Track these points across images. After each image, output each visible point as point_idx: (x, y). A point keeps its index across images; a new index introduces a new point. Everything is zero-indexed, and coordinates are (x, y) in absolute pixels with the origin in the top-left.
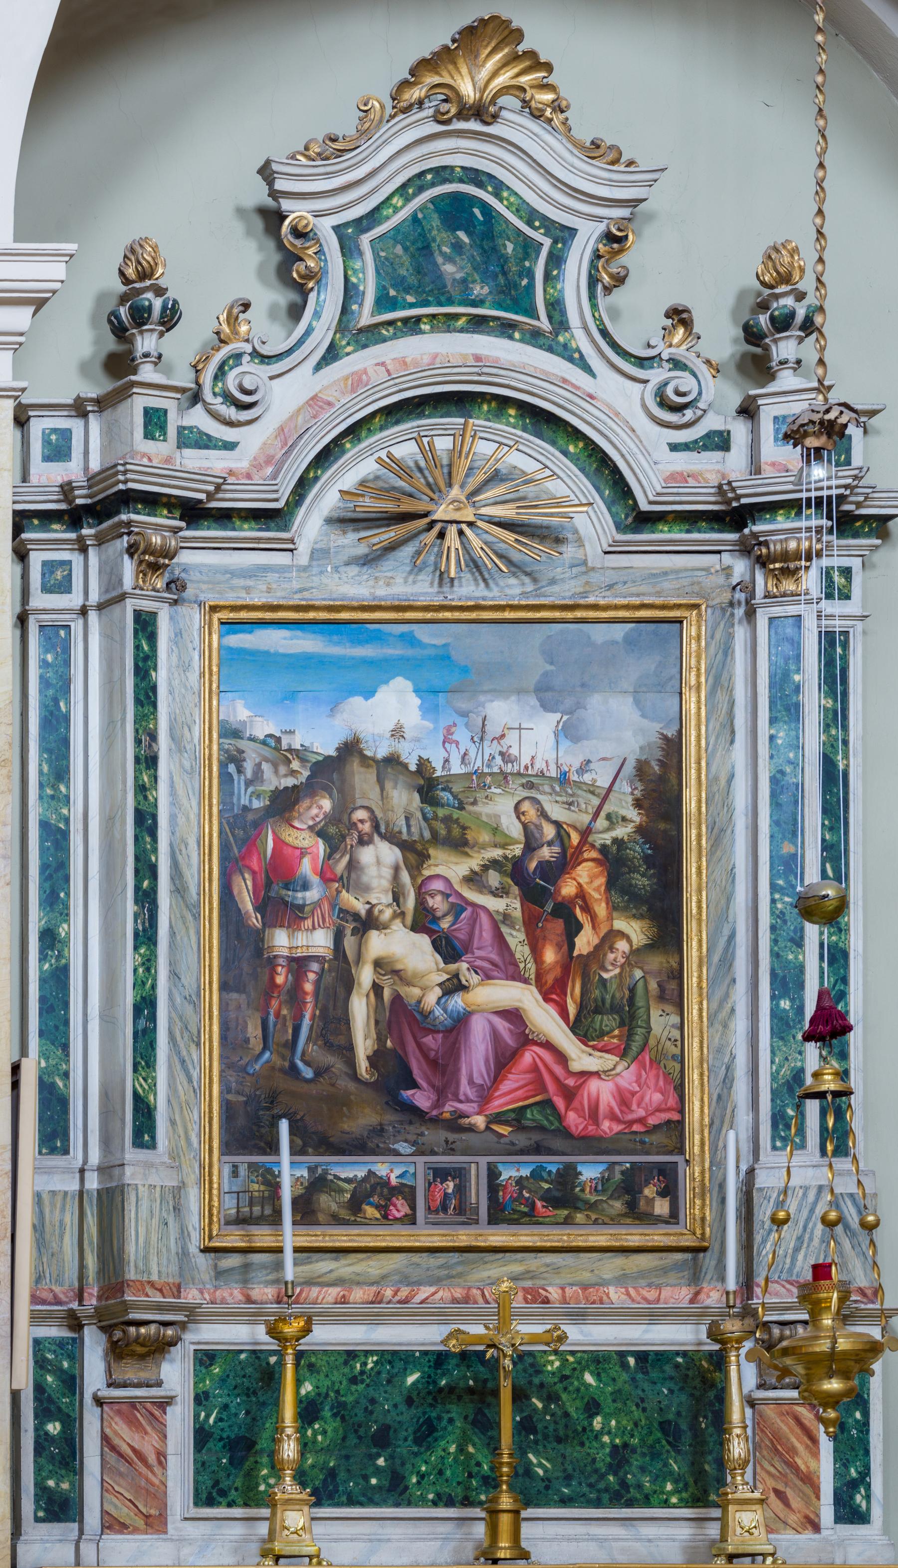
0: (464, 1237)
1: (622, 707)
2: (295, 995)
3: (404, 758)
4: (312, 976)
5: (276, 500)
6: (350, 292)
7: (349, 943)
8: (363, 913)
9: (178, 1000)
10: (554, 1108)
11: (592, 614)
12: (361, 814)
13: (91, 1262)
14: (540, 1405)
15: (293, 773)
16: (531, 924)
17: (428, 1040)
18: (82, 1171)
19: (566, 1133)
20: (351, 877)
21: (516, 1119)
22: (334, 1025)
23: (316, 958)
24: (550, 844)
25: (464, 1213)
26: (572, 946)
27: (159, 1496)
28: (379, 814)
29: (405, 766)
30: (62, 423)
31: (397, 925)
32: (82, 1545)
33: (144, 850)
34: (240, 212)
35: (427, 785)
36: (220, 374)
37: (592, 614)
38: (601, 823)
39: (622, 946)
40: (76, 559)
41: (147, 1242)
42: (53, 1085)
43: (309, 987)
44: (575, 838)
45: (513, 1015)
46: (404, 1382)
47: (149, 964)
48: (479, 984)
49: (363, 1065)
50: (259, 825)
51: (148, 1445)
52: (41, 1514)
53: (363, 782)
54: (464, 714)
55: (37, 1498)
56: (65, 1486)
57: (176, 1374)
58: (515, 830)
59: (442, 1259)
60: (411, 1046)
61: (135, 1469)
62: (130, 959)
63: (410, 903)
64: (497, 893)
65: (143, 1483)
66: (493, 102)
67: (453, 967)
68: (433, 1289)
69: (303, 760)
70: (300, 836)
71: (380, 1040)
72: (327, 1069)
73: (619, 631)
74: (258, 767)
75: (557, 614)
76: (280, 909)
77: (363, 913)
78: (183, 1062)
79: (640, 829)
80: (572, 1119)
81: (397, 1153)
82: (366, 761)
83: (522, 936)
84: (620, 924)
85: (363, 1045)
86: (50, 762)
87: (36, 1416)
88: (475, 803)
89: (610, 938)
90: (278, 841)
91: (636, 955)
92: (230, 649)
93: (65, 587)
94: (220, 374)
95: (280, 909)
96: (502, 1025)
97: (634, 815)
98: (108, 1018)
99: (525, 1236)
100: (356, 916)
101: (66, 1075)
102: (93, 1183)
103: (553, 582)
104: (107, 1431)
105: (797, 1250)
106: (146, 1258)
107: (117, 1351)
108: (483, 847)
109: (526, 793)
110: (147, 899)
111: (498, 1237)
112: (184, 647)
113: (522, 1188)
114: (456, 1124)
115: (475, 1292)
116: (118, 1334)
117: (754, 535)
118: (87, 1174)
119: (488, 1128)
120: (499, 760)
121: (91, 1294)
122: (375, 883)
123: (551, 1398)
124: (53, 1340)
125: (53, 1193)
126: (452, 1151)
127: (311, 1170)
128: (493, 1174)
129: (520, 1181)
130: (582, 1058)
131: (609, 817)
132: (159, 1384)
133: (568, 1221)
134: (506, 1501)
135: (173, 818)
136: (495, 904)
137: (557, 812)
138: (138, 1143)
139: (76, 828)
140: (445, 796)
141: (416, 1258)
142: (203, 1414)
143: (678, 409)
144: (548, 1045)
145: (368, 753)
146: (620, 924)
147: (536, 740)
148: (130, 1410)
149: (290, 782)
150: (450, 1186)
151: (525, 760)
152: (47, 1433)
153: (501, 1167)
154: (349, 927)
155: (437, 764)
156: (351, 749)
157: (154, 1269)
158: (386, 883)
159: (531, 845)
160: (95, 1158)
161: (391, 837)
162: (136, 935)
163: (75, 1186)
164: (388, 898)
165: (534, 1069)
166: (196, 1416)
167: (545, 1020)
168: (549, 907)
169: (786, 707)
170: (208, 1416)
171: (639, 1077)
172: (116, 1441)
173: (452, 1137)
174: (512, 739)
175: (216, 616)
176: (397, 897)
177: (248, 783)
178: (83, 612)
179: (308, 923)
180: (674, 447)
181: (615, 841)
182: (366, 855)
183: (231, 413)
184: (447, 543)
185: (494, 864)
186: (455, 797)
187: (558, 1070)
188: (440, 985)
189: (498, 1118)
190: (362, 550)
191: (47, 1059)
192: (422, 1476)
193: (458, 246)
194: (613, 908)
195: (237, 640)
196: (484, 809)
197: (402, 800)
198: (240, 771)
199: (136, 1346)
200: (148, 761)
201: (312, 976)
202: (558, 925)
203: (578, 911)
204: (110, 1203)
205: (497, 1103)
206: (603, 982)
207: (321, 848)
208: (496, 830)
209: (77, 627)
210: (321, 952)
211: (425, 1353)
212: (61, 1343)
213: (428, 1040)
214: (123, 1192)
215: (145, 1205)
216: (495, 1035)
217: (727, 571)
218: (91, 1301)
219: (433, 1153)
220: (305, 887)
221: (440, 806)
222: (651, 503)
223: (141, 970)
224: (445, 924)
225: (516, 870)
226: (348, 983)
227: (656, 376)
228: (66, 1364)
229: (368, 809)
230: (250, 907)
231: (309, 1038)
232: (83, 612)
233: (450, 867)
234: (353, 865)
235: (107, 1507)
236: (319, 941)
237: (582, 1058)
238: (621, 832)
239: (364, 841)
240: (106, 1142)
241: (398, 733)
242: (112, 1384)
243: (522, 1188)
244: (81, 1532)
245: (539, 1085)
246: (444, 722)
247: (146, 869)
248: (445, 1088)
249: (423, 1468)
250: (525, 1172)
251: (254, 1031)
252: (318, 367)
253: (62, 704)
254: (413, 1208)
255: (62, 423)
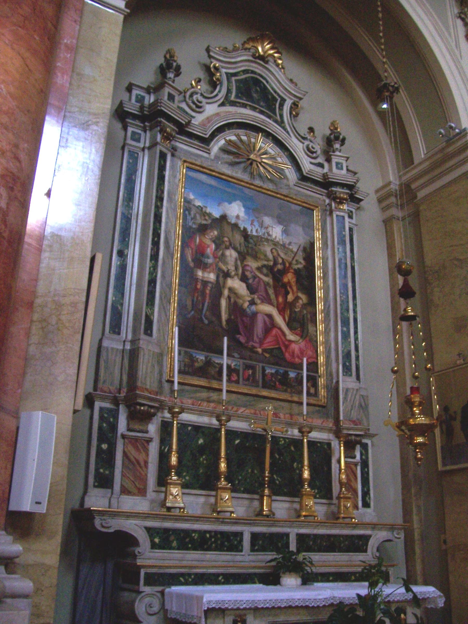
0: (254, 391)
1: (300, 230)
2: (203, 293)
3: (240, 225)
4: (209, 288)
5: (205, 134)
6: (229, 91)
7: (221, 279)
8: (226, 271)
9: (164, 285)
10: (282, 351)
11: (291, 200)
12: (226, 239)
13: (125, 378)
14: (277, 456)
15: (206, 220)
16: (275, 287)
17: (244, 319)
18: (124, 342)
19: (284, 359)
20: (223, 258)
21: (270, 351)
22: (215, 307)
23: (210, 282)
24: (281, 264)
25: (254, 383)
26: (287, 298)
27: (144, 480)
28: (231, 239)
29: (240, 228)
30: (143, 94)
31: (236, 278)
32: (112, 499)
33: (156, 228)
34: (199, 63)
35: (245, 235)
36: (191, 96)
37: (291, 200)
38: (294, 262)
39: (300, 302)
40: (143, 134)
41: (146, 373)
42: (117, 308)
43: (208, 292)
44: (287, 265)
45: (270, 316)
46: (234, 442)
47: (155, 267)
48: (260, 304)
49: (224, 323)
50: (194, 234)
51: (141, 457)
52: (96, 484)
53: (227, 229)
54: (257, 218)
55: (95, 478)
56: (107, 472)
57: (153, 428)
58: (271, 257)
59: (248, 398)
60: (239, 320)
61: (135, 467)
62: (148, 264)
63: (240, 271)
64: (266, 275)
65: (138, 474)
66: (267, 57)
67: (252, 296)
68: (244, 409)
69: (210, 217)
70: (207, 240)
71: (230, 315)
72: (212, 322)
73: (299, 208)
74: (195, 214)
75: (282, 197)
76: (200, 262)
77: (226, 271)
78: (164, 308)
79: (304, 267)
80: (287, 355)
81: (233, 357)
82: (229, 223)
83: (273, 291)
84: (300, 295)
85: (224, 316)
86: (127, 194)
87: (98, 440)
88: (259, 245)
89: (297, 298)
90: (200, 240)
91: (304, 306)
92: (189, 176)
93: (138, 140)
94: (191, 96)
95: (200, 262)
96: (267, 319)
97: (303, 262)
98: (139, 286)
99: (273, 394)
100: (223, 272)
101: (122, 305)
102: (128, 347)
103: (281, 188)
104: (126, 450)
105: (352, 409)
106: (146, 378)
107: (132, 417)
108: (262, 260)
109: (274, 247)
110: (156, 244)
111: (265, 393)
112: (176, 173)
113: (272, 377)
114: (252, 350)
115: (257, 412)
116: (132, 408)
117: (332, 191)
118: (126, 343)
119: (262, 354)
120: (266, 234)
121: (124, 392)
122: (230, 262)
123: (280, 454)
124: (107, 409)
125: (112, 349)
126: (251, 359)
127: (206, 358)
128: (264, 370)
129: (272, 374)
130: (291, 336)
131: (297, 261)
132: (147, 432)
133: (286, 391)
134: (266, 491)
135: (167, 223)
136: (266, 279)
137: (282, 255)
138: (146, 333)
139: (134, 217)
140: (251, 241)
141: (239, 396)
142: (163, 447)
143: (312, 153)
144: (280, 329)
145: (229, 221)
146: (300, 295)
147: (277, 232)
148: (134, 441)
149: (204, 222)
150: (250, 372)
151: (274, 237)
152: (102, 448)
153: (266, 368)
154: (221, 275)
155: (249, 230)
156: (224, 217)
157: (148, 383)
158: (233, 263)
159: (275, 263)
160: (130, 337)
161: (235, 249)
162: (151, 256)
163: (121, 347)
164: (233, 268)
165: (276, 336)
166: (161, 448)
167: (279, 320)
168: (280, 284)
169: (342, 242)
170: (165, 448)
171: (306, 345)
172: (129, 454)
173: (251, 354)
174: (270, 229)
175: (185, 164)
176: (236, 268)
177: (192, 219)
178: (143, 149)
179: (208, 270)
180: (311, 163)
181: (298, 268)
182: (228, 253)
183: (194, 107)
184: (253, 166)
185: (264, 266)
186: (254, 241)
187: (283, 338)
188: (249, 301)
189: (264, 351)
190: (229, 161)
191: (116, 298)
192: (239, 481)
193: (256, 90)
194: (298, 289)
195: (192, 174)
196: (262, 248)
197: (238, 239)
198: (190, 214)
199: (139, 416)
200: (160, 199)
201: (209, 288)
202: (283, 291)
203: (288, 288)
204: (133, 355)
205: (265, 345)
206: (295, 312)
207: (213, 246)
208: (266, 256)
209: (141, 154)
210: (212, 280)
211: (241, 432)
212: (110, 411)
213: (244, 319)
214: (138, 350)
215: (147, 357)
216: (265, 323)
217: (325, 201)
218: (123, 395)
219: (245, 359)
220: (208, 257)
221: (249, 246)
222: (307, 173)
223: (152, 269)
224: (250, 281)
225: (271, 269)
226: (220, 294)
227: (306, 143)
228: (112, 420)
229: (229, 238)
230: (190, 260)
231: (207, 310)
232: (143, 149)
233: (253, 264)
234: (223, 255)
235: (123, 483)
236: (212, 277)
237: (291, 336)
238: (300, 266)
239: (227, 248)
240: (135, 331)
241: (238, 217)
242: (129, 430)
243: (272, 377)
244: (112, 493)
245: (277, 342)
246: (251, 219)
247: (157, 234)
248: (250, 336)
249: (240, 478)
250: (273, 371)
251: (189, 303)
252: (220, 106)
253: (133, 177)
254: (239, 377)
255: (143, 94)
